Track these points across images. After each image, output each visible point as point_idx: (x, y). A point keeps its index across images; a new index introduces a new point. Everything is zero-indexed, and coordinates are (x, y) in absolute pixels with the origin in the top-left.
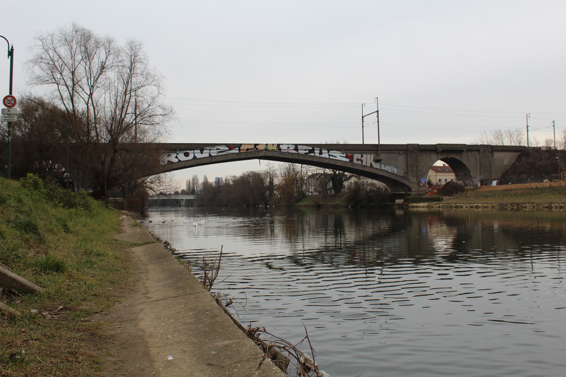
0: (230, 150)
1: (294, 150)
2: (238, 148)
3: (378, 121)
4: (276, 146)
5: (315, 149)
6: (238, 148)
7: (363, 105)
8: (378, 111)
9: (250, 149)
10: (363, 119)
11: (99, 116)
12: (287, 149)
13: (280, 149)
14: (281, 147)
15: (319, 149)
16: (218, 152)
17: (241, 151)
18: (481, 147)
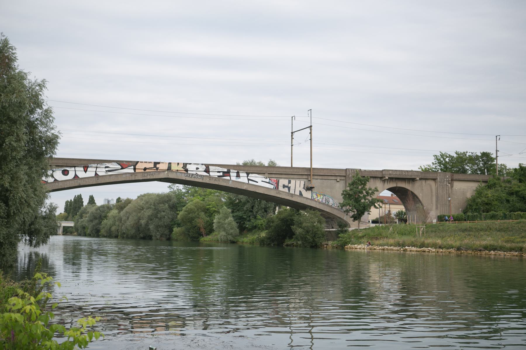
0: (122, 168)
4: (182, 166)
9: (148, 169)
16: (106, 171)
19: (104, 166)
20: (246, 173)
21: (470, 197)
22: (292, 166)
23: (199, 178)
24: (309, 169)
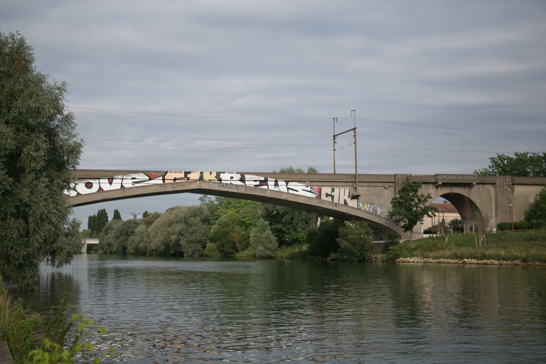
7: (335, 119)
9: (178, 179)
16: (133, 183)
19: (131, 178)
23: (234, 188)
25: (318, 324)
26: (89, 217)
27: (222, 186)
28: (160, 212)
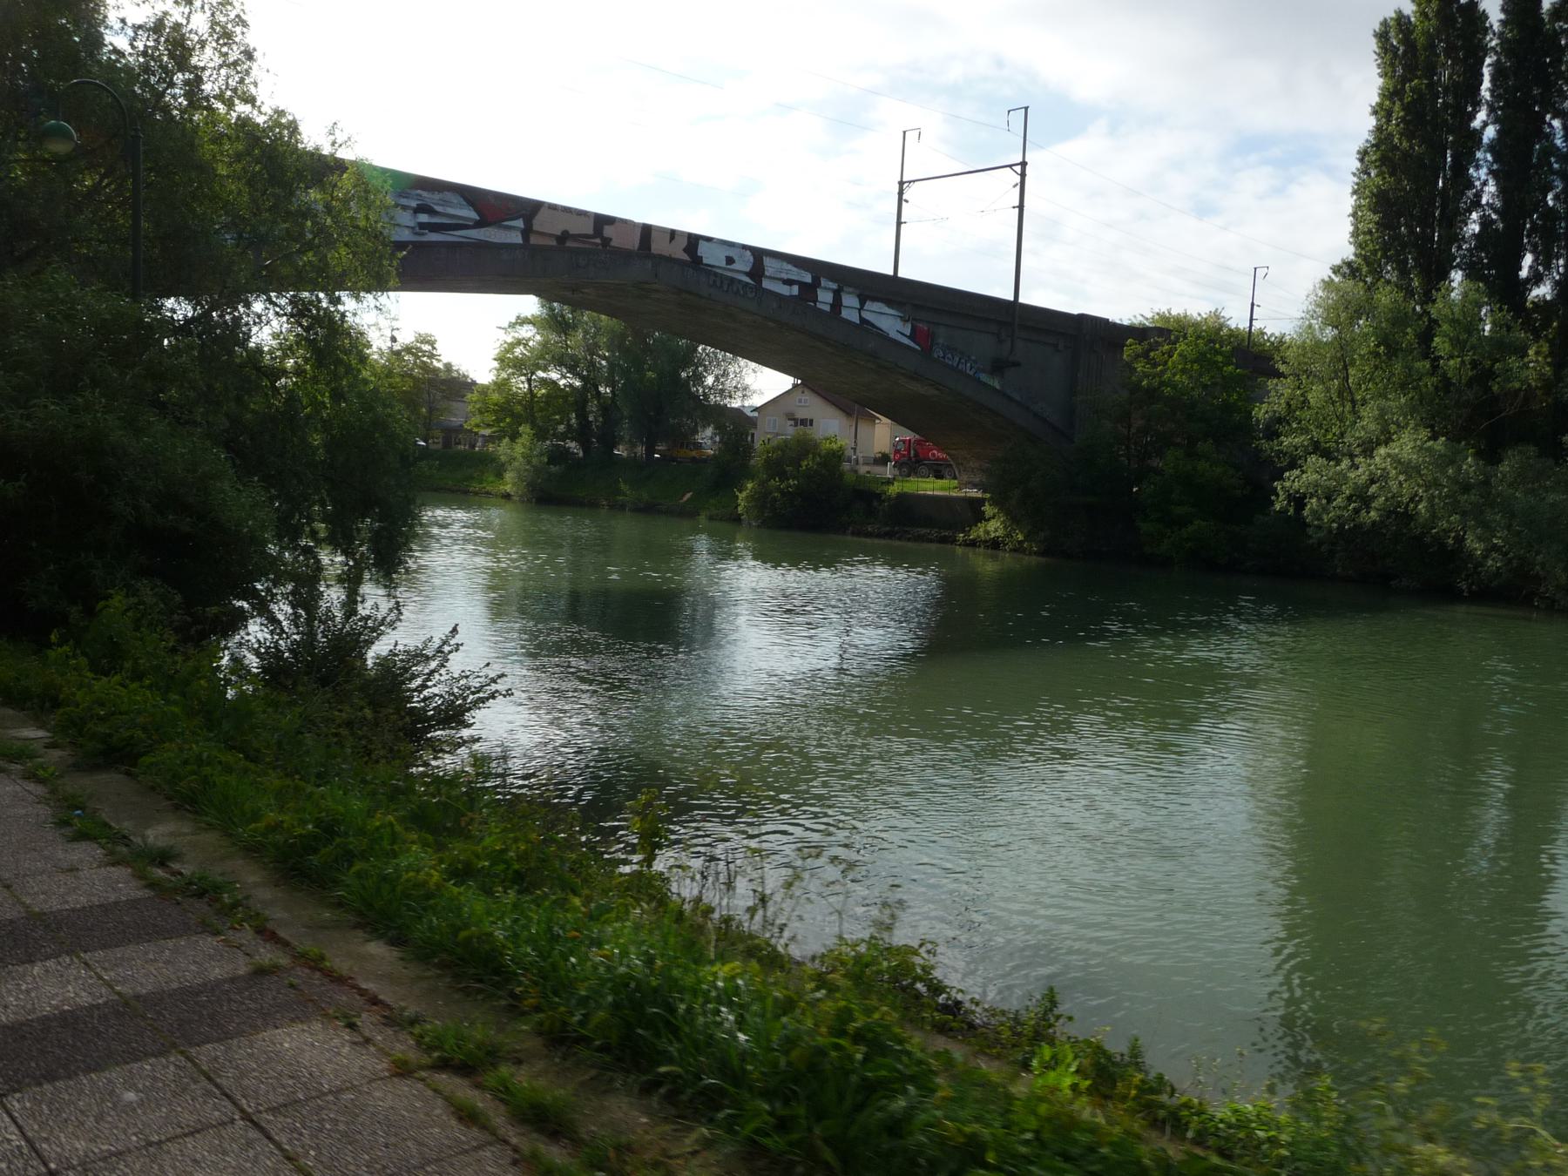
0: (478, 225)
1: (747, 274)
2: (520, 223)
3: (1021, 207)
4: (684, 243)
5: (845, 289)
6: (520, 223)
7: (911, 136)
8: (1024, 164)
9: (576, 237)
10: (901, 193)
11: (1283, 935)
12: (723, 264)
13: (697, 260)
14: (703, 249)
15: (835, 286)
16: (422, 226)
17: (534, 240)
18: (1130, 349)
19: (414, 204)
20: (859, 296)
21: (1381, 80)
22: (767, 277)
23: (750, 296)
24: (841, 305)
25: (498, 658)
26: (1382, 36)
27: (718, 284)
28: (1349, 202)
